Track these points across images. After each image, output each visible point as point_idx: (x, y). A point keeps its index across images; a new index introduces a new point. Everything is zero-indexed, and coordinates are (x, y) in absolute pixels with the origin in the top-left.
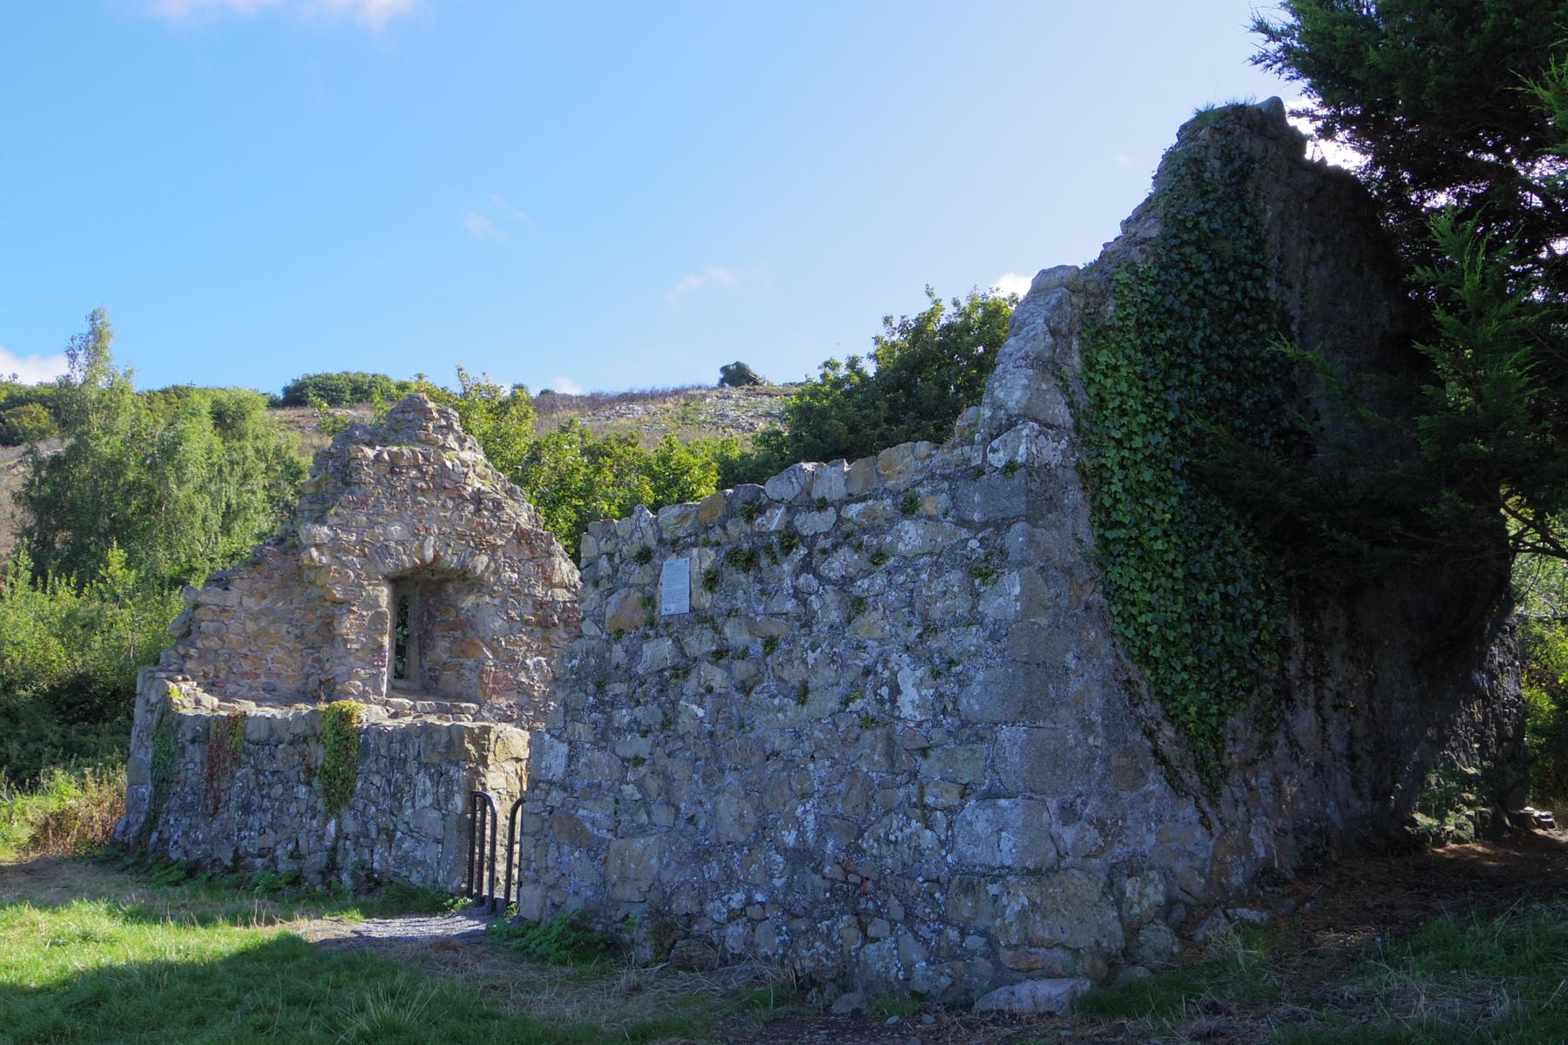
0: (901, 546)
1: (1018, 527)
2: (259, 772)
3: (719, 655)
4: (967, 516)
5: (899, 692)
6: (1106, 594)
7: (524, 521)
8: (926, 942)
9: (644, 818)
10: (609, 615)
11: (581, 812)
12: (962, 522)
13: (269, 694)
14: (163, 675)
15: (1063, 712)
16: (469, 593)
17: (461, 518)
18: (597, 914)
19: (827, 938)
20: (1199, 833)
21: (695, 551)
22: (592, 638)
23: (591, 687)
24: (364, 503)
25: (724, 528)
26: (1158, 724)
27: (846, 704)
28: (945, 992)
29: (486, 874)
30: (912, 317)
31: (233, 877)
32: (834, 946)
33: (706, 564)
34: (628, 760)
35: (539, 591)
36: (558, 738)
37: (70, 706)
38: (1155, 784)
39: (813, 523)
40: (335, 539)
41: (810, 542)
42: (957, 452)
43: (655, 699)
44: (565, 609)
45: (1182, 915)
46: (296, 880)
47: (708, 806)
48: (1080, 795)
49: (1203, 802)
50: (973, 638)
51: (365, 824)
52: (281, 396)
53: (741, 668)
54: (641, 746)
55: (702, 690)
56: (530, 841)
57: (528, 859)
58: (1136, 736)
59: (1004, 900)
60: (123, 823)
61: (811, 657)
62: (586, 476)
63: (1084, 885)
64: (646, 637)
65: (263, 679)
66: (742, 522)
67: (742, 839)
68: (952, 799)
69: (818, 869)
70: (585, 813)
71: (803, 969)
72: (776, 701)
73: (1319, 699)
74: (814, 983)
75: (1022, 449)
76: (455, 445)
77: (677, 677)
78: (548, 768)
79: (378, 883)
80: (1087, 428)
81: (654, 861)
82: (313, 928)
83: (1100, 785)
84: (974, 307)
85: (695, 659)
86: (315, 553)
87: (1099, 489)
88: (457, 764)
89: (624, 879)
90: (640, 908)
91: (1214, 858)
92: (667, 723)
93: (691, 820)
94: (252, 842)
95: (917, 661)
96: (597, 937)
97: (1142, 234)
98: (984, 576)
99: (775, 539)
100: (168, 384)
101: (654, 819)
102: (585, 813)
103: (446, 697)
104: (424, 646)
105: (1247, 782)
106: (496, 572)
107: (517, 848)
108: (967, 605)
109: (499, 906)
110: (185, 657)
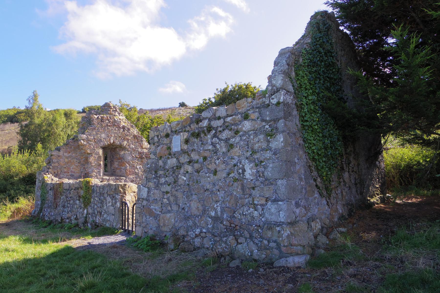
0: (244, 129)
1: (281, 121)
2: (67, 197)
3: (190, 162)
4: (265, 118)
5: (245, 171)
6: (304, 141)
7: (135, 133)
8: (257, 244)
9: (170, 208)
10: (158, 152)
11: (152, 207)
12: (263, 120)
13: (72, 177)
14: (43, 173)
15: (295, 175)
16: (123, 150)
18: (157, 235)
19: (226, 243)
20: (327, 207)
21: (182, 134)
22: (153, 159)
23: (153, 172)
24: (95, 129)
25: (190, 126)
26: (317, 178)
27: (229, 175)
28: (264, 259)
29: (127, 223)
30: (222, 88)
31: (60, 225)
32: (228, 245)
33: (185, 137)
34: (165, 192)
35: (140, 150)
36: (145, 187)
37: (28, 181)
38: (317, 195)
39: (216, 123)
40: (88, 138)
41: (216, 129)
42: (261, 100)
43: (172, 175)
44: (146, 154)
45: (327, 231)
46: (77, 225)
47: (188, 205)
48: (300, 199)
49: (327, 199)
50: (268, 154)
51: (94, 210)
52: (81, 111)
53: (197, 166)
54: (168, 188)
55: (185, 172)
56: (138, 215)
57: (138, 220)
58: (312, 181)
59: (282, 232)
60: (34, 211)
61: (217, 162)
62: (152, 127)
63: (303, 226)
64: (169, 158)
65: (70, 173)
66: (195, 125)
67: (198, 214)
68: (263, 202)
69: (222, 223)
70: (153, 207)
71: (219, 252)
72: (207, 175)
73: (349, 169)
74: (222, 256)
75: (282, 98)
76: (118, 115)
77: (178, 169)
78: (142, 195)
79: (98, 226)
80: (297, 92)
81: (173, 220)
82: (76, 243)
83: (304, 196)
84: (236, 86)
85: (183, 164)
86: (82, 141)
87: (301, 111)
88: (118, 194)
89: (164, 225)
90: (169, 233)
91: (330, 214)
92: (175, 182)
93: (183, 209)
94: (65, 215)
95: (250, 162)
96: (157, 242)
97: (306, 42)
98: (271, 136)
99: (205, 129)
100: (55, 109)
101: (172, 208)
102: (153, 207)
103: (118, 176)
104: (112, 163)
105: (336, 192)
107: (134, 215)
108: (266, 145)
109: (130, 232)
110: (49, 168)
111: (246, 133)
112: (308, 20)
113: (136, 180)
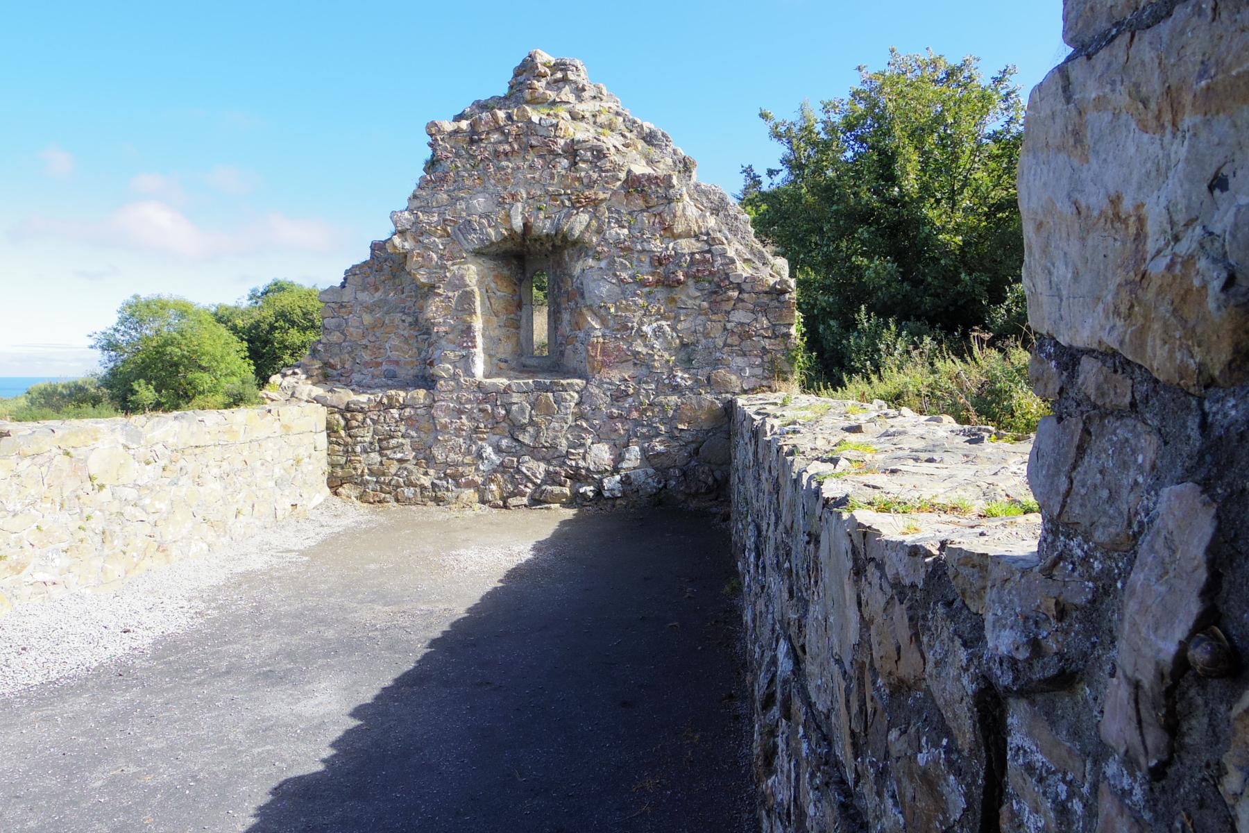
17: (552, 177)
35: (657, 246)
44: (693, 262)
65: (384, 367)
76: (572, 98)
106: (599, 231)
113: (637, 393)
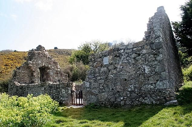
12: (152, 49)
19: (138, 101)
50: (156, 63)
81: (106, 96)
111: (144, 54)
112: (2, 50)
